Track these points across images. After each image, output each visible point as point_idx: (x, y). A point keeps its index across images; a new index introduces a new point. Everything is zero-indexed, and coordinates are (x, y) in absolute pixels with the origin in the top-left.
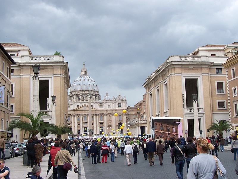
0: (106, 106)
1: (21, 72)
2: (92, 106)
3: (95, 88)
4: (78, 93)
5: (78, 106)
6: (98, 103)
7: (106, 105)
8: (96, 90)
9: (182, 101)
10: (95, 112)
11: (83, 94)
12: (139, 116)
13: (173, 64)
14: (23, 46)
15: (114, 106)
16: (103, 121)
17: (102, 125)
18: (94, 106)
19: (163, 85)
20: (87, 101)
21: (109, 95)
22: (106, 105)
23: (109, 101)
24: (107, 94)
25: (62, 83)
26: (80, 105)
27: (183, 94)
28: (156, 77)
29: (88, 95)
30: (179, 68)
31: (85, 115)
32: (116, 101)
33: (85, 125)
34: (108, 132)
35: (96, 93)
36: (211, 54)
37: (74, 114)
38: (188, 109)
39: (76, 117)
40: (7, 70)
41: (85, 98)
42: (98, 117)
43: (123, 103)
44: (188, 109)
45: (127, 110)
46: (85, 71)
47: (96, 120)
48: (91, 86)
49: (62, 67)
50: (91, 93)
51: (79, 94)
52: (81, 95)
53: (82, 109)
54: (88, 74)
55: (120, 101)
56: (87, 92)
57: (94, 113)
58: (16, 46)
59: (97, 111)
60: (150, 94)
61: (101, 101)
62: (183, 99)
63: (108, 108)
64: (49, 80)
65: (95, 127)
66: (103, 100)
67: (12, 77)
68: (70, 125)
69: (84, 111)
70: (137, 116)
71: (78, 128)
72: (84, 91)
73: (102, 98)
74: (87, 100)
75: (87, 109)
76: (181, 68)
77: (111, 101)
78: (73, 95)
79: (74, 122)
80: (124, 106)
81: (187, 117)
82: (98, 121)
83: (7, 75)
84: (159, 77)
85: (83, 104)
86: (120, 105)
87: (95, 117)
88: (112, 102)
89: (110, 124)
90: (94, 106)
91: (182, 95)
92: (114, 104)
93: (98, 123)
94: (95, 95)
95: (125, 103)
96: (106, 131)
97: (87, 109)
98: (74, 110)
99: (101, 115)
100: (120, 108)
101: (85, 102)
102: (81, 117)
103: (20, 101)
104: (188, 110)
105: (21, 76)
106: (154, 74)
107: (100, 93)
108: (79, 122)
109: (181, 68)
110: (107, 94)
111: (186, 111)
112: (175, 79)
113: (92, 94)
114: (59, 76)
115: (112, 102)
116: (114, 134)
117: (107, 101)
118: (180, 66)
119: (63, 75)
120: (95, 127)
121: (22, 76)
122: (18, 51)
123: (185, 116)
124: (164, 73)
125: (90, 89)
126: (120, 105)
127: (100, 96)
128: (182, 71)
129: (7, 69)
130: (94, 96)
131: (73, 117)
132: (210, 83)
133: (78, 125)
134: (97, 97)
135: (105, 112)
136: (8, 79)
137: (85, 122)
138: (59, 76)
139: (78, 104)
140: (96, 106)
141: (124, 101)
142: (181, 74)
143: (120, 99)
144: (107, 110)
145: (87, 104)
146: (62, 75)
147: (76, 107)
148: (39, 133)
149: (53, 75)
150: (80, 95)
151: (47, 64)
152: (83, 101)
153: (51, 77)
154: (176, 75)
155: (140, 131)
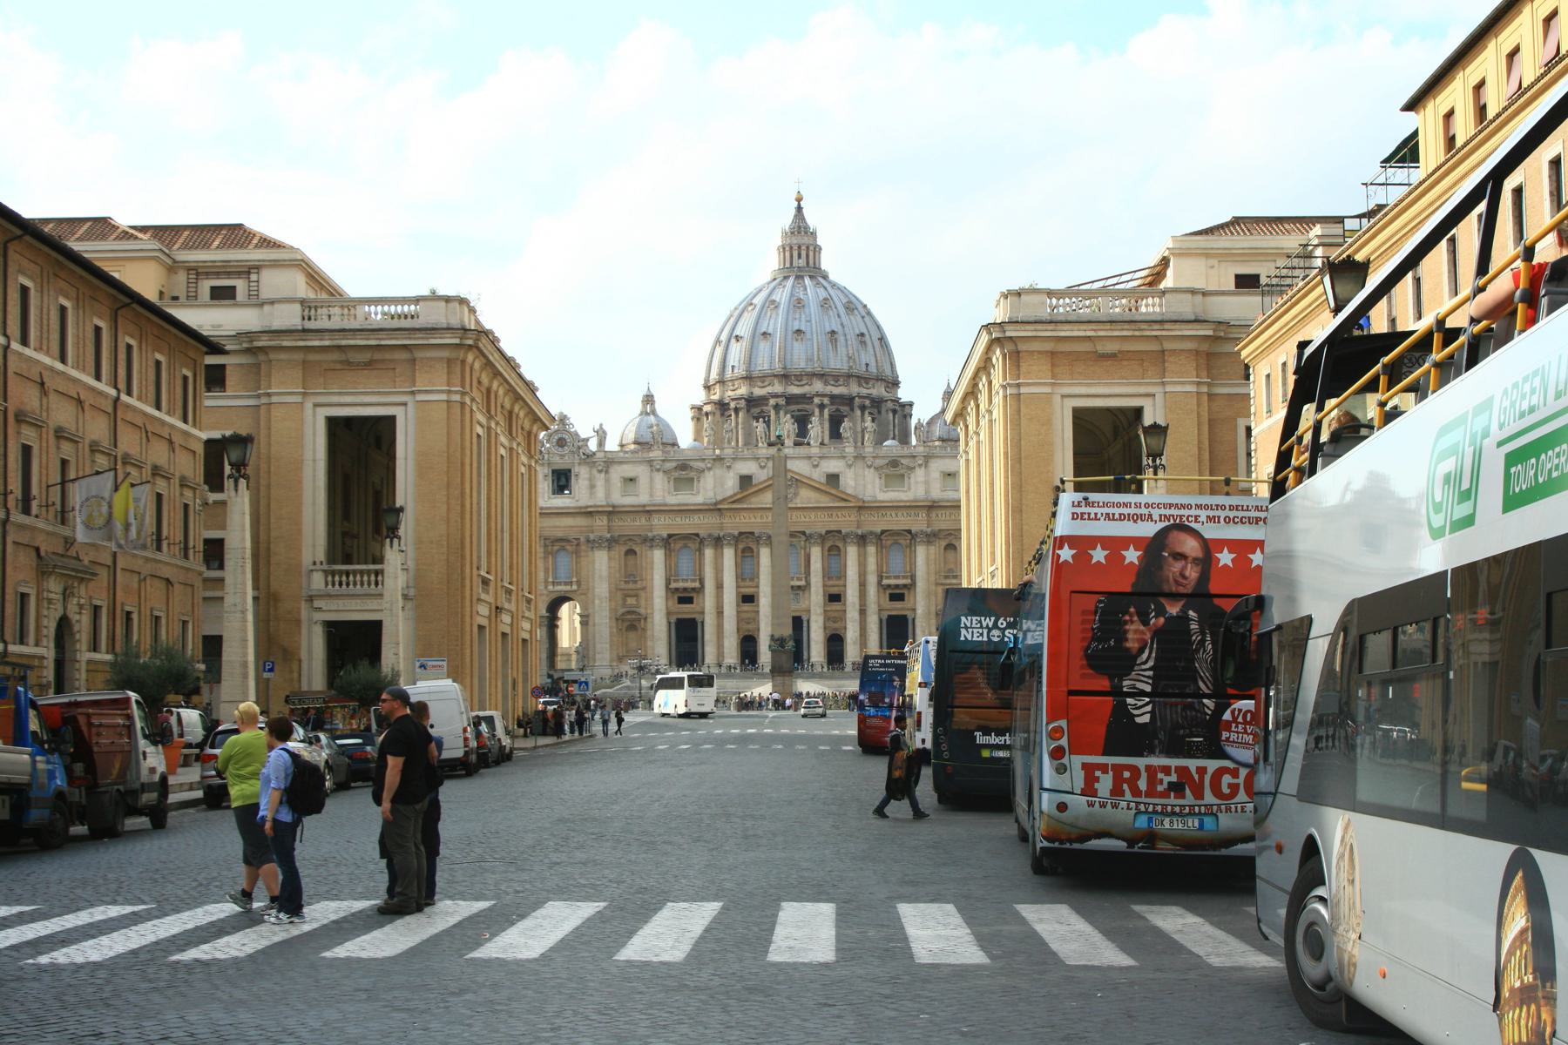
0: (927, 483)
2: (833, 478)
4: (758, 392)
5: (745, 480)
7: (927, 474)
11: (791, 399)
13: (1008, 334)
16: (697, 585)
17: (898, 604)
18: (852, 483)
22: (927, 474)
35: (878, 391)
36: (1237, 277)
37: (716, 533)
39: (729, 554)
40: (179, 390)
42: (871, 549)
48: (842, 350)
50: (837, 391)
56: (818, 386)
57: (846, 522)
63: (619, 499)
64: (392, 419)
65: (852, 614)
68: (689, 600)
71: (831, 624)
72: (799, 377)
78: (722, 406)
79: (719, 586)
82: (872, 579)
83: (179, 411)
87: (852, 552)
88: (650, 462)
89: (631, 601)
90: (849, 482)
93: (872, 590)
94: (867, 402)
98: (715, 508)
107: (903, 394)
112: (1019, 411)
113: (849, 401)
114: (444, 397)
115: (650, 462)
121: (264, 400)
122: (249, 273)
125: (837, 363)
128: (1057, 370)
129: (179, 382)
130: (863, 408)
131: (709, 553)
132: (1206, 428)
133: (747, 607)
135: (918, 523)
138: (444, 397)
140: (863, 483)
147: (730, 485)
149: (413, 393)
150: (772, 402)
153: (405, 404)
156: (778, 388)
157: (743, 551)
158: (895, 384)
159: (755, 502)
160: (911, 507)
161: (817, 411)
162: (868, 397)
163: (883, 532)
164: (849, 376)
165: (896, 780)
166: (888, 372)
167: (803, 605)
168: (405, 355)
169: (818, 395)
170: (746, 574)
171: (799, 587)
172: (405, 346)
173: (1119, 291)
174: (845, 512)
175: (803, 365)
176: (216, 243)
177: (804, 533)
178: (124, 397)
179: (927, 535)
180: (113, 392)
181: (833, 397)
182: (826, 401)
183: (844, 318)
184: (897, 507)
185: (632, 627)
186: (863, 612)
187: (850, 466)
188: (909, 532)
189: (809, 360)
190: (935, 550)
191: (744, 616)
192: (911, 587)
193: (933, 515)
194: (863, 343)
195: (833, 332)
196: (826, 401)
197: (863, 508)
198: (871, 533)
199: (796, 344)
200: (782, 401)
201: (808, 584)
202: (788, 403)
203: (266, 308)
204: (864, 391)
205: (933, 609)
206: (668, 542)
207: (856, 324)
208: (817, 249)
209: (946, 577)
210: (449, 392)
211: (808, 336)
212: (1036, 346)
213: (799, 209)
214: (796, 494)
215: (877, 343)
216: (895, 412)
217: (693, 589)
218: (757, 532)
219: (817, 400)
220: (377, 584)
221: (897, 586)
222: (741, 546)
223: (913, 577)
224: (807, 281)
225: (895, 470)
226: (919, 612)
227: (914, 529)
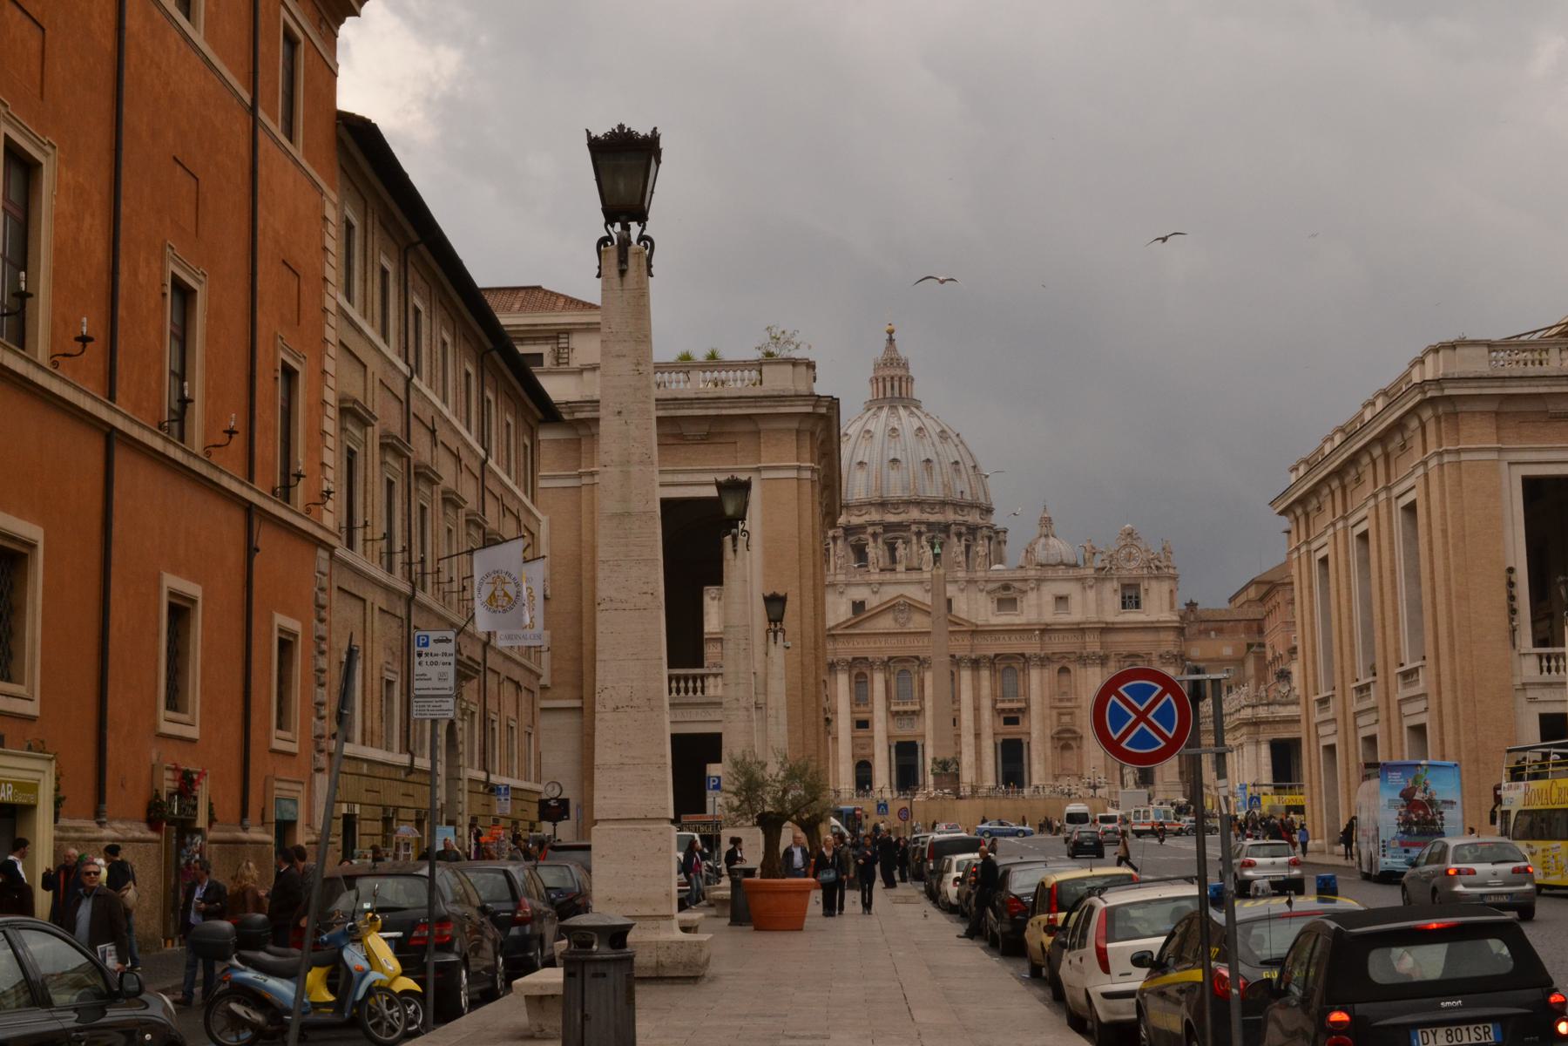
0: (1039, 606)
1: (580, 459)
3: (962, 487)
5: (858, 607)
6: (991, 586)
8: (968, 497)
9: (1505, 596)
10: (967, 641)
11: (888, 527)
12: (1258, 670)
13: (1447, 392)
14: (584, 304)
15: (1092, 606)
16: (1022, 705)
18: (965, 607)
19: (1390, 513)
20: (915, 576)
21: (1056, 527)
23: (1061, 572)
24: (1046, 522)
25: (808, 515)
26: (873, 602)
27: (1511, 570)
28: (1353, 460)
29: (919, 534)
30: (1482, 413)
31: (904, 667)
32: (1102, 575)
33: (905, 732)
34: (1056, 777)
35: (974, 518)
38: (1540, 656)
41: (901, 551)
42: (985, 674)
43: (1154, 584)
44: (1540, 656)
45: (1180, 631)
46: (899, 372)
47: (976, 694)
48: (938, 478)
49: (807, 425)
50: (933, 518)
51: (861, 528)
52: (875, 535)
53: (886, 623)
54: (917, 392)
55: (1132, 569)
56: (915, 514)
57: (962, 647)
58: (542, 307)
59: (979, 641)
60: (1320, 554)
61: (1008, 575)
62: (1512, 598)
63: (1050, 616)
65: (968, 739)
66: (1021, 561)
67: (542, 484)
69: (893, 641)
70: (1250, 667)
73: (1014, 551)
74: (915, 564)
75: (918, 622)
76: (1497, 413)
77: (1071, 572)
80: (1157, 607)
81: (1533, 700)
82: (986, 703)
84: (1366, 460)
85: (890, 593)
86: (1131, 599)
87: (966, 676)
89: (1066, 719)
90: (961, 607)
91: (1504, 573)
92: (1091, 594)
93: (987, 715)
94: (964, 529)
95: (1166, 586)
96: (1038, 768)
97: (918, 622)
99: (1008, 666)
100: (1133, 616)
101: (901, 576)
102: (878, 681)
103: (580, 621)
104: (1545, 663)
105: (580, 476)
106: (1338, 440)
107: (997, 520)
108: (862, 708)
109: (1497, 413)
110: (1046, 522)
111: (1529, 669)
112: (1460, 483)
113: (945, 528)
114: (794, 474)
116: (1095, 787)
117: (1050, 573)
118: (1493, 406)
119: (813, 470)
120: (968, 739)
121: (586, 480)
123: (1521, 700)
124: (1398, 440)
125: (933, 491)
126: (1131, 599)
127: (997, 537)
130: (959, 535)
133: (861, 732)
134: (981, 548)
135: (1031, 647)
136: (527, 502)
137: (901, 708)
139: (859, 594)
140: (976, 608)
141: (1160, 570)
142: (1500, 450)
143: (1129, 558)
144: (1046, 630)
145: (916, 593)
146: (806, 468)
148: (1522, 932)
149: (758, 470)
150: (870, 530)
151: (724, 412)
152: (888, 576)
154: (1464, 457)
155: (1270, 768)
156: (875, 516)
157: (857, 676)
158: (989, 511)
159: (868, 628)
160: (1024, 631)
161: (914, 539)
162: (964, 524)
163: (996, 656)
164: (943, 504)
165: (1127, 913)
166: (982, 500)
167: (918, 729)
168: (749, 427)
169: (915, 522)
170: (861, 696)
171: (914, 712)
172: (749, 416)
173: (1524, 344)
174: (959, 637)
175: (899, 494)
176: (517, 306)
177: (917, 658)
178: (491, 463)
179: (1041, 659)
180: (482, 452)
181: (929, 525)
182: (923, 528)
183: (939, 447)
184: (1010, 631)
185: (1066, 747)
186: (977, 736)
187: (962, 590)
188: (1023, 655)
189: (904, 489)
190: (1051, 672)
191: (860, 741)
192: (1024, 711)
193: (1046, 638)
194: (958, 471)
195: (928, 461)
196: (923, 528)
197: (976, 632)
198: (985, 657)
199: (893, 473)
200: (879, 530)
201: (923, 709)
202: (885, 531)
203: (586, 375)
204: (959, 518)
205: (1048, 733)
206: (886, 664)
207: (950, 452)
208: (910, 380)
209: (1061, 700)
210: (799, 468)
211: (904, 461)
212: (1479, 407)
213: (891, 340)
214: (909, 619)
215: (971, 471)
216: (990, 538)
217: (1019, 710)
218: (870, 656)
219: (914, 528)
220: (1557, 670)
221: (1011, 710)
222: (854, 672)
223: (1027, 701)
224: (902, 411)
225: (1007, 597)
226: (1034, 735)
227: (1028, 652)
